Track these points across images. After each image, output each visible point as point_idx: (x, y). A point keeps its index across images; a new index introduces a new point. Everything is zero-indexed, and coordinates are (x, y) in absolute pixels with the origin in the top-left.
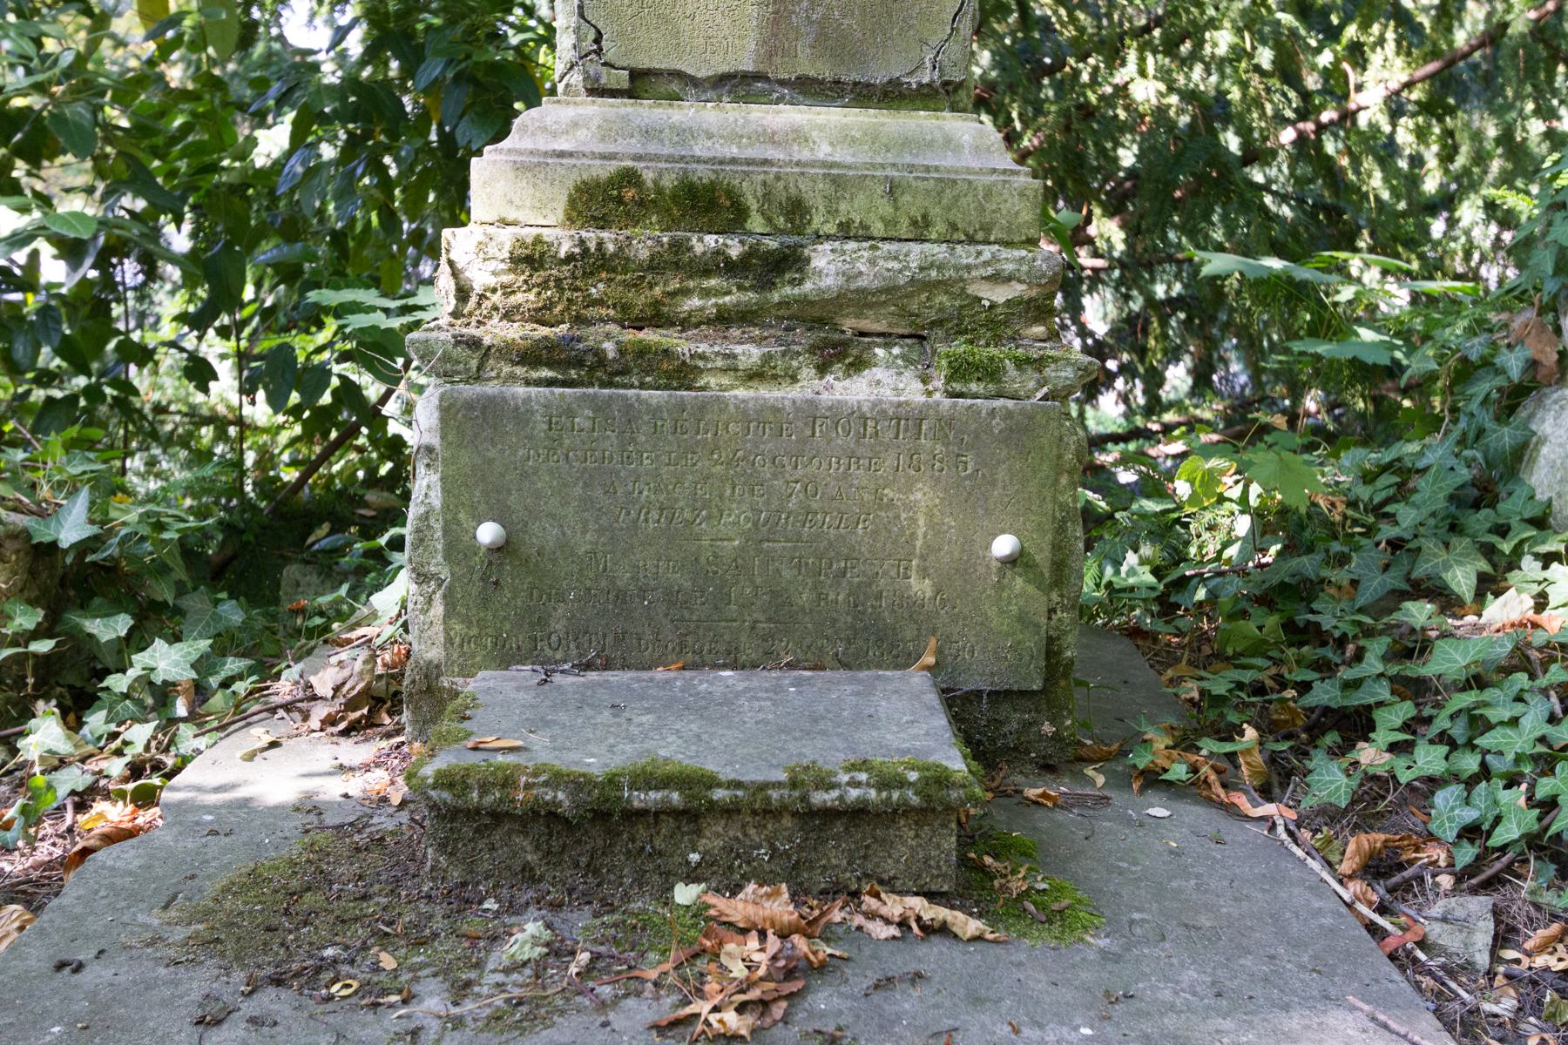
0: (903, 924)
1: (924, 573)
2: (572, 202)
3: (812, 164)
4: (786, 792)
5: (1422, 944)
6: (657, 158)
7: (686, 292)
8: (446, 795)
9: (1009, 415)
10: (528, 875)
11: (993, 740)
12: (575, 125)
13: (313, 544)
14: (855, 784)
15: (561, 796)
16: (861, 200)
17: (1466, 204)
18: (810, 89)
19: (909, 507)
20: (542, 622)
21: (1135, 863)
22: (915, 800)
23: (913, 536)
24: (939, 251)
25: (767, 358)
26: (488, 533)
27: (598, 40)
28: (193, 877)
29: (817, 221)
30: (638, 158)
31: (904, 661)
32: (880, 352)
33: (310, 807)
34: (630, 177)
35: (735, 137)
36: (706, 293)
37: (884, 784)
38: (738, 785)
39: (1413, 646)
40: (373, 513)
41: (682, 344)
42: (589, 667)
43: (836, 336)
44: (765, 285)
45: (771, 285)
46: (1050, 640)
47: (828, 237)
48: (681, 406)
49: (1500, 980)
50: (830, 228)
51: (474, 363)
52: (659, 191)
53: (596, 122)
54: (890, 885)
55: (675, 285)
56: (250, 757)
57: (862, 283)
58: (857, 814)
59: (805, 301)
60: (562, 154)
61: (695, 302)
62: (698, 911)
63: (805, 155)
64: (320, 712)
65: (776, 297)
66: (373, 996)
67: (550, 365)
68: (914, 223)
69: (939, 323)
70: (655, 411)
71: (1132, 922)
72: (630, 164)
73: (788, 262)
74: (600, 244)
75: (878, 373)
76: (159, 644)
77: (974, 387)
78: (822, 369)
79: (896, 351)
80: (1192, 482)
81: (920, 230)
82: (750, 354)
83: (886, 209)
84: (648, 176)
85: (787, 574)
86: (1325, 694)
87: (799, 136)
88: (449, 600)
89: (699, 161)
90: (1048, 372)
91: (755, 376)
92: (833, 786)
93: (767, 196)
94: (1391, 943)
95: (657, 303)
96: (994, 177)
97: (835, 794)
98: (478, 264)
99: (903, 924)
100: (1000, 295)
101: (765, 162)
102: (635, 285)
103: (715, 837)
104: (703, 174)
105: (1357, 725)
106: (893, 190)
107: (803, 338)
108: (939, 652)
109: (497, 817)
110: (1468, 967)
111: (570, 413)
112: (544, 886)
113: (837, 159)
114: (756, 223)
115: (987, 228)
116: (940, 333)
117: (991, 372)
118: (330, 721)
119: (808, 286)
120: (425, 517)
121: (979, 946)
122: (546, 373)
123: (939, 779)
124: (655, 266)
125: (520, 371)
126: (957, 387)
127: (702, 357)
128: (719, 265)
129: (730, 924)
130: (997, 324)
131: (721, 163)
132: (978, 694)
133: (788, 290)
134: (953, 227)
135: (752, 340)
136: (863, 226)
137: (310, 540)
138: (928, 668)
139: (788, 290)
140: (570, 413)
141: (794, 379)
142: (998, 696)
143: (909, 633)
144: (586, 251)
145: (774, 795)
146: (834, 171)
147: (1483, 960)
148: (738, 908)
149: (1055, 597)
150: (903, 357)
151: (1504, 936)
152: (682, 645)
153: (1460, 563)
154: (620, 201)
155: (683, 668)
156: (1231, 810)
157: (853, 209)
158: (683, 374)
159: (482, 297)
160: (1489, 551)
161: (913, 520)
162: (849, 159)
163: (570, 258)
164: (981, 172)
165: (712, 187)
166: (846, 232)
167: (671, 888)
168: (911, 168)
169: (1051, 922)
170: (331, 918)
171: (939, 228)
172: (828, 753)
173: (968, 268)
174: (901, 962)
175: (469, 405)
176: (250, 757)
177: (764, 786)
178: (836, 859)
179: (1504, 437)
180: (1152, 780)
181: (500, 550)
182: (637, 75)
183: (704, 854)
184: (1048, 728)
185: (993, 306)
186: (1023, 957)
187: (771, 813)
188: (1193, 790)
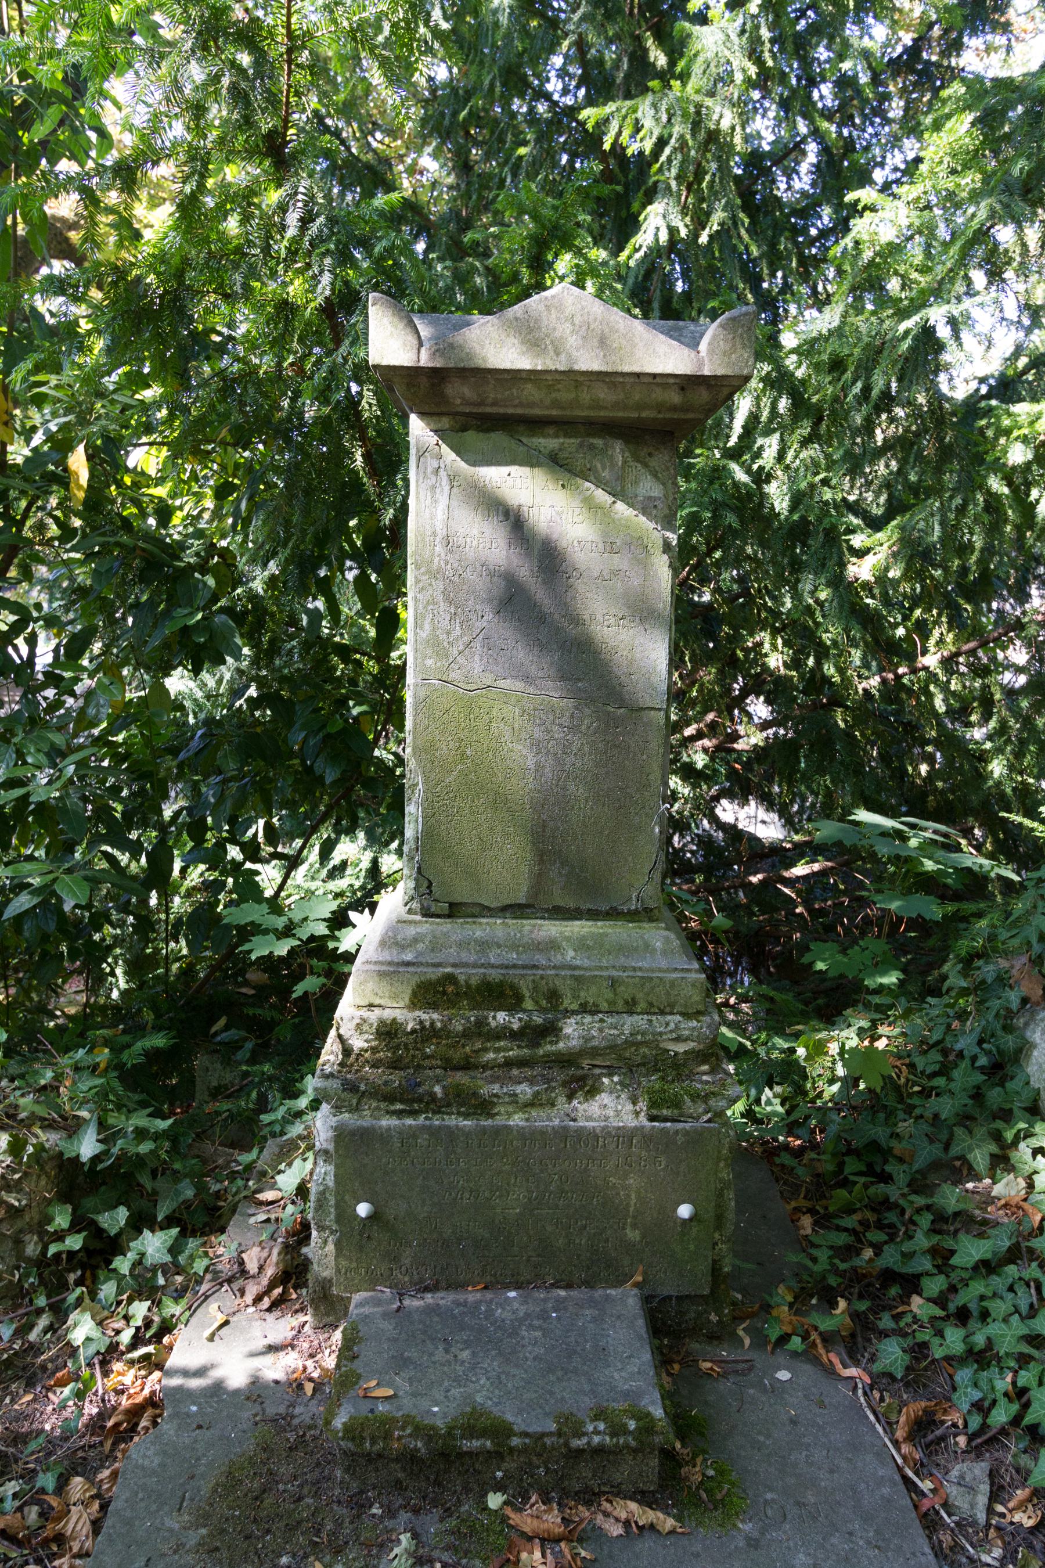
0: (627, 1524)
1: (634, 1226)
2: (414, 994)
3: (563, 967)
4: (554, 1439)
5: (945, 1505)
6: (466, 965)
7: (486, 1050)
8: (350, 1445)
9: (687, 1133)
11: (679, 1324)
12: (415, 940)
13: (216, 1034)
14: (597, 1432)
15: (419, 1444)
16: (594, 989)
17: (995, 762)
19: (626, 1188)
20: (396, 1259)
21: (768, 1436)
22: (633, 1444)
23: (628, 1205)
24: (639, 1021)
25: (536, 1094)
26: (363, 1209)
27: (429, 886)
28: (192, 1477)
29: (567, 1003)
30: (455, 965)
32: (606, 1080)
33: (256, 1385)
34: (451, 979)
35: (514, 947)
36: (498, 1050)
38: (526, 1435)
40: (252, 992)
41: (487, 1090)
42: (427, 1289)
43: (580, 1072)
44: (535, 1044)
45: (538, 1045)
46: (714, 1262)
47: (574, 1013)
48: (484, 1130)
49: (992, 1533)
50: (575, 1006)
51: (354, 1101)
52: (468, 986)
53: (429, 938)
54: (619, 1493)
55: (478, 1045)
56: (211, 1338)
57: (595, 1043)
59: (559, 1053)
60: (408, 964)
61: (491, 1055)
63: (558, 959)
64: (252, 1290)
65: (541, 1052)
67: (401, 1102)
68: (627, 1003)
69: (644, 1064)
70: (467, 1134)
71: (766, 1502)
72: (448, 970)
73: (550, 1030)
74: (432, 1023)
75: (604, 1098)
76: (147, 1233)
77: (665, 1112)
78: (570, 1097)
79: (616, 1079)
80: (807, 1047)
82: (525, 1091)
83: (610, 995)
84: (462, 978)
85: (549, 1229)
86: (890, 1258)
87: (552, 945)
88: (338, 1245)
89: (493, 966)
90: (712, 1102)
92: (584, 1434)
93: (535, 989)
94: (926, 1504)
95: (467, 1057)
96: (674, 975)
97: (585, 1440)
98: (356, 1035)
99: (627, 1524)
100: (681, 1048)
101: (535, 967)
102: (454, 1046)
104: (495, 975)
106: (614, 983)
108: (645, 1274)
110: (974, 1523)
111: (415, 1136)
112: (409, 1494)
113: (578, 963)
114: (528, 1004)
115: (672, 1005)
116: (643, 1070)
119: (561, 1045)
120: (322, 1193)
121: (673, 1538)
122: (399, 1106)
124: (467, 1034)
125: (383, 1105)
126: (655, 1112)
127: (496, 1095)
128: (503, 1033)
129: (523, 1534)
131: (507, 967)
132: (670, 1297)
133: (548, 1047)
134: (651, 1005)
135: (526, 1079)
136: (595, 1005)
137: (213, 1030)
138: (636, 1285)
139: (548, 1047)
140: (415, 1136)
141: (553, 1105)
143: (626, 1261)
144: (423, 1028)
145: (548, 1441)
146: (577, 973)
147: (981, 1517)
149: (717, 1236)
150: (621, 1083)
152: (484, 1272)
153: (979, 1146)
154: (444, 993)
155: (486, 1288)
156: (830, 1371)
157: (588, 995)
158: (484, 1107)
159: (359, 1055)
160: (997, 1137)
161: (628, 1196)
162: (586, 963)
163: (414, 1031)
164: (667, 971)
165: (501, 984)
166: (585, 1009)
167: (486, 1495)
168: (624, 969)
169: (716, 1508)
170: (282, 1524)
171: (642, 1005)
173: (661, 1034)
175: (353, 1133)
176: (211, 1338)
177: (543, 1435)
178: (587, 1473)
181: (372, 1217)
182: (452, 905)
183: (505, 1472)
184: (714, 1318)
185: (676, 1054)
186: (698, 1547)
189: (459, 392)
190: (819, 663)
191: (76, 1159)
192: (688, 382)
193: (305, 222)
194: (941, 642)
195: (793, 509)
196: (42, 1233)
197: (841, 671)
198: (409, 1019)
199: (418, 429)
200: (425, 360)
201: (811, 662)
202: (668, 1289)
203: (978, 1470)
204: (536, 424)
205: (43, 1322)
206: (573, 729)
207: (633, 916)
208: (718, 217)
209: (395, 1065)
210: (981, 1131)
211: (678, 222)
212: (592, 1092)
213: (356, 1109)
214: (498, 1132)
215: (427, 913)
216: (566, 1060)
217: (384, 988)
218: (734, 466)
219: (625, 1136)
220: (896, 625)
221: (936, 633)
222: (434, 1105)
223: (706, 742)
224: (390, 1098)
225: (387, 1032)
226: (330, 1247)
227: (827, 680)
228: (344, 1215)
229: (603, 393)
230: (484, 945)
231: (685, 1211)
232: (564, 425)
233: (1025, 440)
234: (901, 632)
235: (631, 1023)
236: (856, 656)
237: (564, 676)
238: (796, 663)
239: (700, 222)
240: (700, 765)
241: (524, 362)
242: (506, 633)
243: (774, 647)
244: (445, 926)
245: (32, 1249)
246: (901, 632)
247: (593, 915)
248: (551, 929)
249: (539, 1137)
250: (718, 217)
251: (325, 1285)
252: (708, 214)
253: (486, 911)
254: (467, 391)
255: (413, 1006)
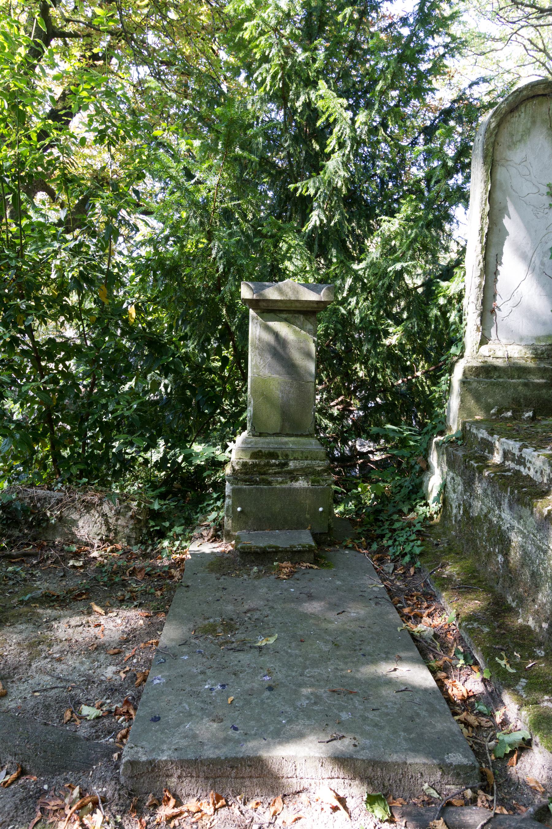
10: (253, 562)
18: (288, 435)
24: (309, 462)
26: (239, 509)
29: (290, 457)
31: (305, 528)
33: (213, 553)
34: (260, 451)
35: (276, 443)
37: (303, 547)
39: (392, 522)
41: (270, 479)
44: (282, 468)
58: (299, 552)
62: (278, 565)
64: (206, 539)
66: (238, 576)
73: (286, 464)
81: (306, 458)
82: (280, 479)
87: (286, 443)
91: (281, 483)
100: (320, 469)
103: (279, 555)
104: (272, 450)
105: (382, 536)
106: (302, 452)
107: (288, 476)
109: (249, 553)
117: (318, 482)
118: (209, 540)
123: (311, 546)
124: (265, 465)
128: (274, 465)
130: (319, 473)
142: (321, 534)
148: (284, 564)
151: (395, 569)
156: (359, 552)
157: (296, 455)
158: (269, 483)
160: (411, 505)
166: (295, 459)
172: (295, 543)
174: (306, 571)
179: (418, 481)
180: (346, 547)
181: (241, 512)
187: (287, 552)
188: (353, 548)
189: (262, 304)
190: (376, 375)
191: (154, 510)
192: (318, 302)
193: (218, 252)
194: (423, 367)
195: (360, 323)
196: (147, 527)
197: (383, 377)
198: (250, 462)
199: (252, 312)
200: (255, 297)
201: (373, 374)
202: (316, 531)
203: (392, 565)
204: (281, 311)
205: (150, 548)
206: (291, 387)
207: (307, 436)
208: (337, 218)
209: (246, 474)
210: (406, 503)
211: (323, 217)
212: (297, 480)
213: (237, 484)
214: (273, 489)
215: (254, 436)
216: (290, 472)
217: (243, 454)
218: (341, 308)
219: (305, 490)
220: (406, 361)
221: (421, 363)
222: (257, 483)
223: (339, 407)
224: (245, 481)
225: (244, 465)
226: (230, 521)
227: (378, 380)
228: (234, 511)
229: (298, 304)
230: (269, 443)
231: (321, 509)
232: (288, 311)
233: (444, 296)
234: (408, 363)
235: (306, 462)
236: (388, 371)
237: (289, 373)
238: (369, 375)
239: (330, 219)
240: (336, 414)
241: (279, 298)
242: (274, 363)
243: (361, 369)
244: (258, 439)
245: (144, 531)
246: (408, 363)
247: (297, 436)
248: (286, 439)
249: (284, 490)
250: (337, 218)
251: (229, 532)
252: (334, 216)
253: (269, 435)
254: (264, 304)
255: (251, 458)
